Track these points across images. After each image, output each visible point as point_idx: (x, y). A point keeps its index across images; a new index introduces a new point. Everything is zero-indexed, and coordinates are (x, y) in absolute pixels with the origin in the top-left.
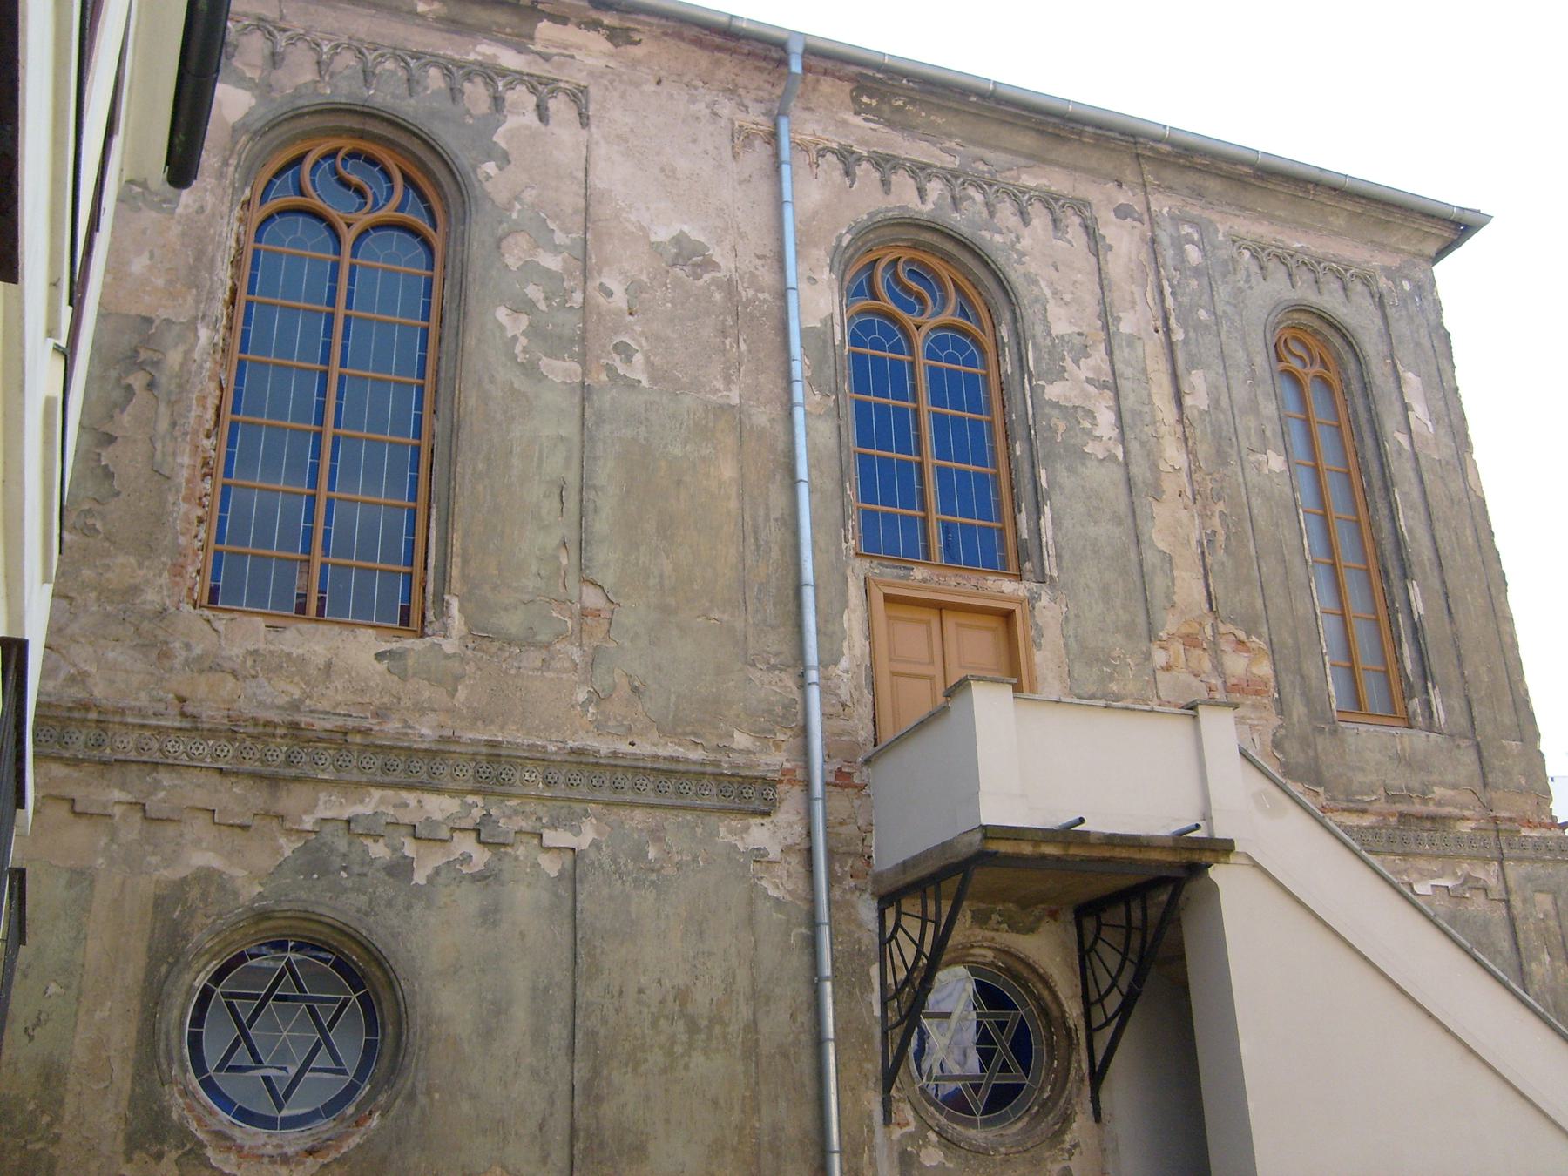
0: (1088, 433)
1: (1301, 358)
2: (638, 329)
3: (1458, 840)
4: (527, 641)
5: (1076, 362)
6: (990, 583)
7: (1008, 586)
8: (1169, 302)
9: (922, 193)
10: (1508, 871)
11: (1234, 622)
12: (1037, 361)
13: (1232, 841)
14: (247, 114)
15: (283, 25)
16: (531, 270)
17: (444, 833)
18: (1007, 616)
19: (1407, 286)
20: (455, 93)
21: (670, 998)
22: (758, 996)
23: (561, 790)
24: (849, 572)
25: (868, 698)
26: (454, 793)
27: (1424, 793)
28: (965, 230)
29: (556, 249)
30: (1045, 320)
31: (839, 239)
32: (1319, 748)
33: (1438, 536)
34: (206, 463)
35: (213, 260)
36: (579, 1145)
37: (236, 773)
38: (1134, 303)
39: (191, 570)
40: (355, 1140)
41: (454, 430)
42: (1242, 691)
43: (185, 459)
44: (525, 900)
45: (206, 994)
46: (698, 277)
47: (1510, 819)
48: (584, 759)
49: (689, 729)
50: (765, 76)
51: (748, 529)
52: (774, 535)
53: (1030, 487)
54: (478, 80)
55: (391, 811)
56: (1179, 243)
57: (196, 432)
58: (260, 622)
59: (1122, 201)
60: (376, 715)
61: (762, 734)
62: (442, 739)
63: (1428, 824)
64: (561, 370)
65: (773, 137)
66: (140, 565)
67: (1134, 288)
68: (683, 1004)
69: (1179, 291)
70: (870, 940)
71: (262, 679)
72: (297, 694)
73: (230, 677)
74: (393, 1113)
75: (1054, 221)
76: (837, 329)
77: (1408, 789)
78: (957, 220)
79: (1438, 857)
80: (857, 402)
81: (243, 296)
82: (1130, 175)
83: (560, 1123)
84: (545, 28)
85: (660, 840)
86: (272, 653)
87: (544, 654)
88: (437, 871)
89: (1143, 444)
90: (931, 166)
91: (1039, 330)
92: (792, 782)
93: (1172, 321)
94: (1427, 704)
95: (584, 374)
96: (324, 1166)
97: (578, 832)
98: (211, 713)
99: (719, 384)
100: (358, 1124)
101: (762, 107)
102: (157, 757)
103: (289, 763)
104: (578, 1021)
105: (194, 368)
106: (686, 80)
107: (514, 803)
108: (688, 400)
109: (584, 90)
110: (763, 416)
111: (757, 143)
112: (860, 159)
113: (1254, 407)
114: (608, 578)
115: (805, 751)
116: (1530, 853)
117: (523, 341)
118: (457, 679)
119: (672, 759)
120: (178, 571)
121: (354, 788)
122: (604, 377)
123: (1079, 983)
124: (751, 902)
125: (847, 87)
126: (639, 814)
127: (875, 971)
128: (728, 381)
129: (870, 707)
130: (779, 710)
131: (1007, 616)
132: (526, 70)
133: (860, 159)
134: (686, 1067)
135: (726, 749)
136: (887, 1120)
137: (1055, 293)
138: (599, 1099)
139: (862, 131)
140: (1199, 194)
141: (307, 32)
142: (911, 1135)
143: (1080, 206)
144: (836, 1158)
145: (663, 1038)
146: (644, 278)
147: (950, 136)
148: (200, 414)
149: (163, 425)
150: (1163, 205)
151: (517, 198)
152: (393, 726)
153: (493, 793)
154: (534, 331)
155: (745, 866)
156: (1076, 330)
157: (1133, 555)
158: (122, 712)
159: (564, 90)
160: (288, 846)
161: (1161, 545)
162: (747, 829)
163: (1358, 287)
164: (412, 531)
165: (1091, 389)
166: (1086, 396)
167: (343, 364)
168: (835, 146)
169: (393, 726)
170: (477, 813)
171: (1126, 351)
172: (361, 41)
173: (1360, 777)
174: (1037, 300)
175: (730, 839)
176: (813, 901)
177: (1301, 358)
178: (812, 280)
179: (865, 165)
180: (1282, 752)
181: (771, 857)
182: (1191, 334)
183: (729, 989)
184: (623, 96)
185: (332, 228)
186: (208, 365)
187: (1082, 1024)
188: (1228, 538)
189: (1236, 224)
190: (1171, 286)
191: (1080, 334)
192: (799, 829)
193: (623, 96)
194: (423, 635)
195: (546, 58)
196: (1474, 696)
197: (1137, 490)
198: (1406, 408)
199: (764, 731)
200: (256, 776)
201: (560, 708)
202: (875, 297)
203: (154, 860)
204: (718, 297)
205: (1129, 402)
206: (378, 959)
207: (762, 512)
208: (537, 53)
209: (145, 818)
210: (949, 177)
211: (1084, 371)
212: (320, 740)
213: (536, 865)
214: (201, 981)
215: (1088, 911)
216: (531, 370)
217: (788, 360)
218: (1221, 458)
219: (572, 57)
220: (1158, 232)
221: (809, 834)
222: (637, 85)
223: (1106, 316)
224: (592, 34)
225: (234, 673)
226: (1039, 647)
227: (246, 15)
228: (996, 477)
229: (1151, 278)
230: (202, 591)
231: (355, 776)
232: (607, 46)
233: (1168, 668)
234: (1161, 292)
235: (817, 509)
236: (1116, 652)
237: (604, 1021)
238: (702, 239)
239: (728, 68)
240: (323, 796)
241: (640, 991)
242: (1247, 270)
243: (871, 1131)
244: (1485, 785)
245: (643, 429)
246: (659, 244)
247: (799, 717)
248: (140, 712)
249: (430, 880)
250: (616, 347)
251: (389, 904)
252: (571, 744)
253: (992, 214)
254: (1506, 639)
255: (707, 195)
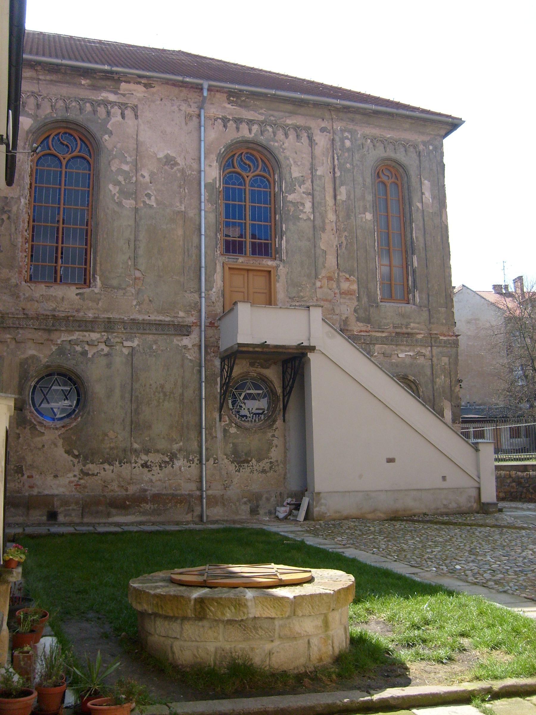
0: (302, 211)
1: (388, 176)
2: (153, 188)
3: (416, 341)
4: (119, 288)
5: (300, 187)
6: (264, 262)
7: (270, 263)
8: (336, 162)
9: (250, 130)
10: (433, 350)
11: (345, 272)
12: (286, 188)
13: (315, 347)
14: (31, 127)
15: (39, 94)
16: (120, 171)
17: (96, 343)
18: (270, 272)
19: (431, 148)
20: (95, 112)
21: (159, 387)
22: (184, 386)
23: (128, 330)
24: (217, 262)
25: (222, 299)
26: (98, 332)
27: (407, 326)
28: (264, 143)
29: (127, 163)
30: (290, 173)
31: (220, 151)
32: (371, 312)
33: (427, 239)
34: (26, 239)
35: (24, 177)
36: (133, 426)
37: (39, 329)
38: (323, 164)
39: (24, 271)
40: (75, 424)
41: (97, 225)
42: (346, 294)
43: (20, 240)
44: (118, 361)
45: (35, 387)
46: (172, 168)
47: (436, 334)
48: (135, 321)
49: (166, 311)
50: (197, 94)
51: (186, 250)
52: (194, 251)
53: (280, 230)
54: (102, 106)
55: (81, 338)
56: (342, 141)
57: (22, 231)
58: (43, 286)
59: (323, 126)
60: (76, 311)
61: (187, 312)
62: (95, 318)
63: (406, 336)
64: (129, 203)
65: (199, 116)
66: (10, 272)
67: (324, 158)
68: (162, 389)
69: (340, 158)
70: (218, 370)
71: (45, 303)
72: (55, 306)
73: (36, 302)
74: (84, 417)
75: (297, 136)
76: (218, 182)
77: (401, 324)
78: (262, 139)
79: (408, 346)
80: (226, 204)
81: (34, 185)
82: (327, 115)
83: (128, 419)
84: (123, 85)
85: (157, 343)
86: (47, 295)
87: (124, 291)
88: (94, 354)
89: (320, 214)
90: (253, 120)
91: (288, 176)
92: (196, 326)
93: (336, 170)
94: (414, 296)
95: (136, 204)
96: (67, 430)
97: (133, 342)
98: (31, 313)
99: (178, 204)
100: (75, 420)
101: (196, 105)
102: (18, 326)
103: (53, 326)
104: (133, 393)
105: (20, 211)
106: (170, 98)
107: (115, 334)
108: (168, 211)
109: (136, 106)
110: (191, 213)
111: (194, 118)
112: (229, 120)
113: (363, 197)
114: (142, 268)
115: (200, 316)
116: (443, 344)
117: (117, 195)
118: (99, 300)
119: (160, 321)
120: (20, 273)
121: (70, 332)
122: (142, 205)
123: (282, 383)
124: (183, 360)
125: (225, 95)
126: (151, 336)
127: (219, 379)
128: (181, 203)
129: (222, 302)
130: (193, 305)
131: (270, 272)
132: (118, 101)
133: (229, 120)
134: (163, 405)
135: (177, 317)
136: (220, 421)
137: (295, 162)
138: (139, 414)
139: (231, 110)
140: (353, 120)
141: (47, 96)
142: (227, 424)
143: (307, 129)
144: (204, 430)
145: (157, 398)
146: (155, 171)
147: (262, 108)
148: (23, 225)
149: (13, 230)
150: (338, 126)
151: (115, 147)
152: (81, 314)
153: (109, 332)
154: (121, 192)
155: (181, 350)
156: (301, 175)
157: (313, 252)
158: (8, 314)
159: (130, 107)
160: (54, 348)
161: (323, 248)
162: (182, 340)
163: (412, 149)
164: (86, 255)
165: (304, 196)
166: (302, 198)
167: (64, 205)
168: (220, 117)
169: (81, 314)
170: (105, 337)
171: (318, 181)
172: (64, 97)
173: (385, 321)
174: (288, 165)
175: (177, 343)
176: (200, 360)
177: (388, 176)
178: (210, 166)
179: (231, 122)
180: (357, 313)
181: (189, 347)
182: (343, 173)
183: (175, 384)
184: (149, 106)
185: (59, 159)
186: (24, 210)
187: (282, 394)
188: (347, 244)
189: (365, 130)
190: (338, 156)
191: (302, 176)
192: (198, 339)
193: (149, 106)
194: (90, 287)
195: (124, 95)
196: (431, 294)
197: (317, 229)
198: (423, 194)
199: (188, 311)
200: (44, 330)
201: (128, 307)
202: (234, 167)
203: (19, 353)
204: (179, 175)
205: (318, 199)
206: (79, 377)
207: (190, 244)
208: (122, 94)
209: (16, 342)
210: (261, 123)
211: (302, 189)
212: (61, 319)
213: (122, 351)
214: (33, 384)
215: (285, 363)
216: (120, 204)
217: (200, 195)
218: (348, 217)
219: (133, 94)
220: (335, 136)
221: (200, 341)
222: (153, 101)
223: (313, 169)
224: (139, 86)
225: (37, 301)
226: (278, 282)
227: (28, 91)
228: (271, 226)
229: (331, 154)
230: (27, 277)
231: (71, 328)
232: (144, 89)
233: (321, 287)
234: (334, 159)
235: (208, 244)
236: (304, 283)
237: (140, 393)
238: (174, 155)
239: (185, 92)
240: (63, 334)
241: (151, 385)
242: (368, 147)
243: (216, 423)
244: (430, 323)
245: (154, 221)
246: (160, 158)
247: (199, 306)
248: (12, 314)
249: (93, 356)
250: (146, 195)
251: (82, 363)
252: (131, 317)
253: (275, 136)
254: (447, 274)
255: (176, 139)
